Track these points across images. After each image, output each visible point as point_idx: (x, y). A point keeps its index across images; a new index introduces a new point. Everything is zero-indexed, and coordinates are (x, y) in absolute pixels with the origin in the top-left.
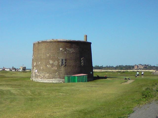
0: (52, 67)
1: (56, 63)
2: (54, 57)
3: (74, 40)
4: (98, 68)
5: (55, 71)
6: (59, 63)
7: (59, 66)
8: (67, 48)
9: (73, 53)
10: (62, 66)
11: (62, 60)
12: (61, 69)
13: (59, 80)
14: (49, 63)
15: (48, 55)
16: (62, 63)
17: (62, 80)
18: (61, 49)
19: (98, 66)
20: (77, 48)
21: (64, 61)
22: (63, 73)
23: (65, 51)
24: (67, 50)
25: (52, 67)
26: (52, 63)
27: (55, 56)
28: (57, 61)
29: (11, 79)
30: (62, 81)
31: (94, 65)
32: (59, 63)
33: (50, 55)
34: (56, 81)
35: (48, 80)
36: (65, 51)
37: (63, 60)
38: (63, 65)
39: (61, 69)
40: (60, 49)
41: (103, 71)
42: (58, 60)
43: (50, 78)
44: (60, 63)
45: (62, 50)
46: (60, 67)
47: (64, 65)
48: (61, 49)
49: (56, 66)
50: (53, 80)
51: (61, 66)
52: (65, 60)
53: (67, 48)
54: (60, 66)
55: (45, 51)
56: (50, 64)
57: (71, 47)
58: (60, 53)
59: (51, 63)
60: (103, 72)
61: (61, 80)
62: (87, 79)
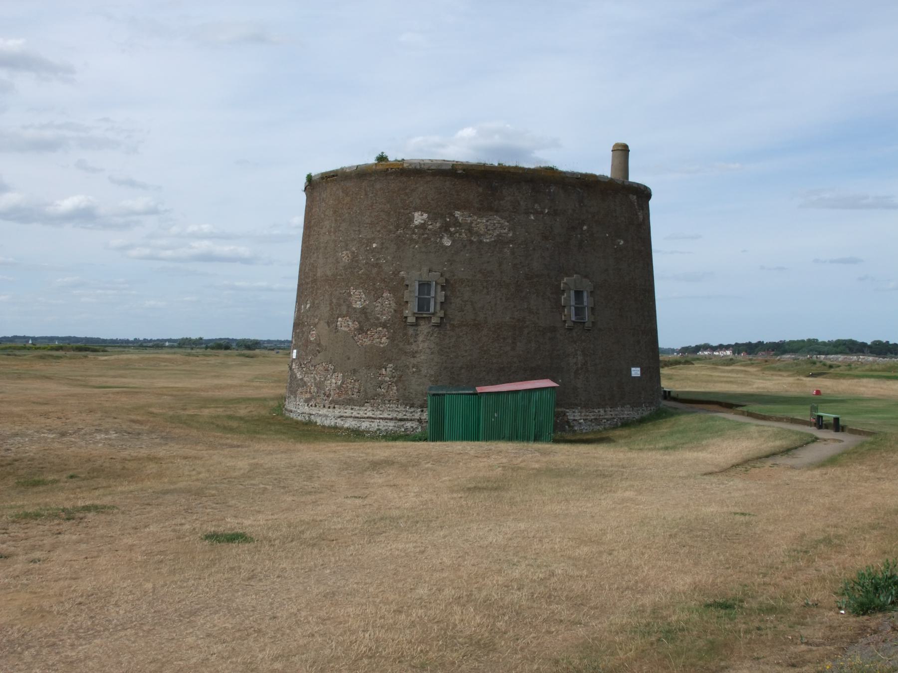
0: (361, 330)
1: (385, 307)
2: (375, 271)
3: (512, 163)
4: (690, 355)
5: (377, 359)
6: (402, 304)
7: (400, 328)
8: (457, 214)
9: (500, 242)
10: (424, 328)
11: (424, 286)
12: (414, 347)
13: (400, 416)
14: (349, 306)
15: (345, 257)
16: (423, 305)
17: (417, 416)
18: (419, 218)
19: (371, 160)
20: (527, 213)
21: (437, 295)
22: (424, 371)
23: (445, 228)
24: (460, 225)
25: (361, 330)
26: (363, 309)
27: (383, 261)
28: (393, 290)
29: (115, 390)
30: (420, 421)
31: (671, 334)
32: (402, 304)
33: (354, 252)
34: (382, 423)
35: (337, 412)
36: (445, 228)
37: (428, 284)
38: (429, 319)
39: (414, 347)
40: (411, 220)
41: (880, 415)
42: (398, 287)
43: (350, 402)
44: (411, 311)
45: (423, 226)
46: (411, 331)
47: (435, 320)
48: (419, 218)
49: (384, 325)
50: (362, 414)
51: (416, 325)
52: (443, 288)
53: (457, 214)
54: (412, 325)
55: (335, 232)
56: (350, 312)
57: (486, 208)
58: (412, 240)
59: (358, 305)
60: (121, 376)
61: (409, 416)
62: (547, 441)
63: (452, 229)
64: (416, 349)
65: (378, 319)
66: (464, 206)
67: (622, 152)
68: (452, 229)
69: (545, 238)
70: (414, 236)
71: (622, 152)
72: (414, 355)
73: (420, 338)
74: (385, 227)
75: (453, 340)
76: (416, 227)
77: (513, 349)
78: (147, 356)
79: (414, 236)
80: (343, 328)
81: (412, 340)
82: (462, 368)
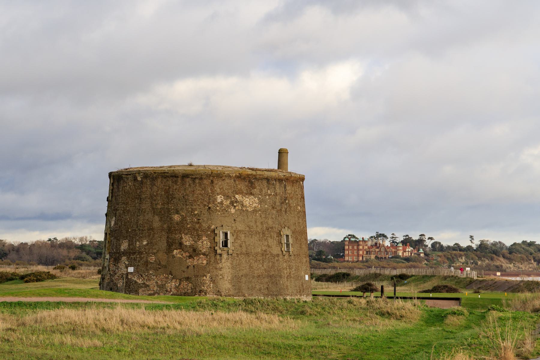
36: (232, 203)
39: (220, 265)
40: (216, 199)
45: (221, 203)
63: (235, 204)
64: (221, 266)
65: (201, 251)
66: (240, 192)
67: (282, 154)
68: (235, 204)
69: (273, 208)
70: (218, 208)
71: (282, 154)
72: (221, 269)
73: (223, 261)
74: (202, 203)
75: (238, 261)
76: (218, 203)
77: (263, 266)
78: (322, 290)
79: (218, 208)
80: (178, 256)
81: (219, 262)
82: (242, 276)
